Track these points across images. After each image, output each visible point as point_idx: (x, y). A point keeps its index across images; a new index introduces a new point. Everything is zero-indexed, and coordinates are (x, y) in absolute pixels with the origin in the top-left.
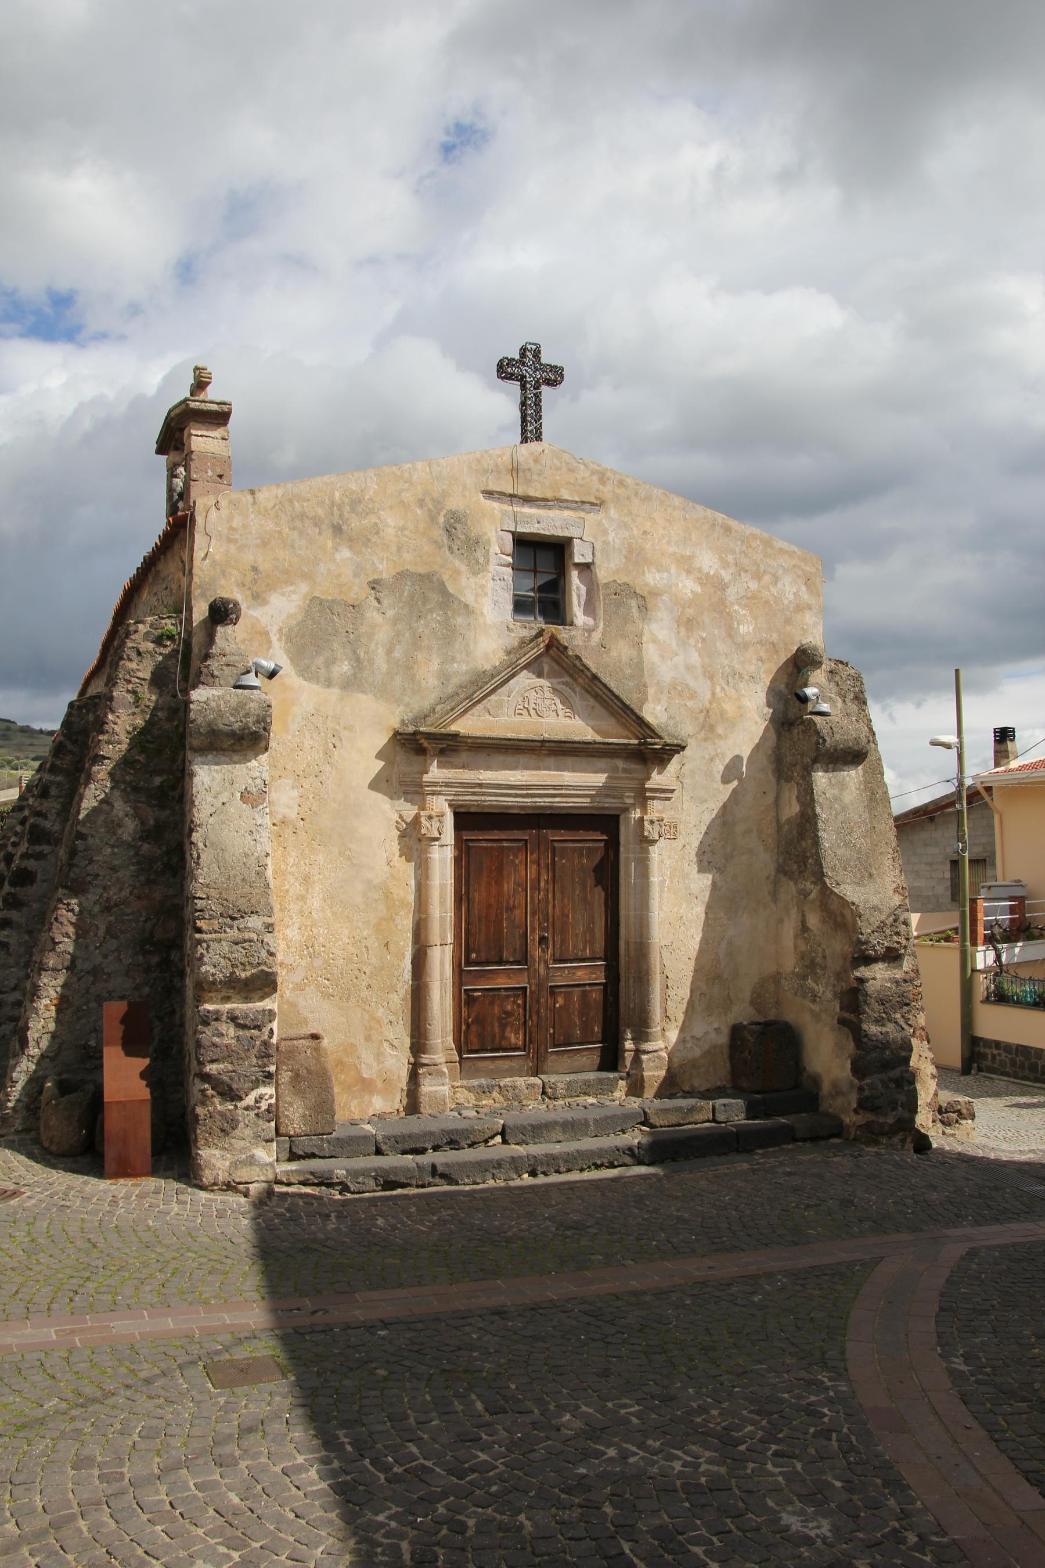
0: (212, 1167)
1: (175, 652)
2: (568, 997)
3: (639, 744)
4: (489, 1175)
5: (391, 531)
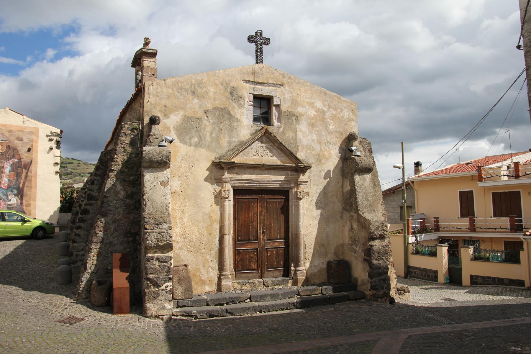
0: (151, 310)
1: (138, 134)
2: (272, 252)
4: (245, 313)
5: (212, 93)
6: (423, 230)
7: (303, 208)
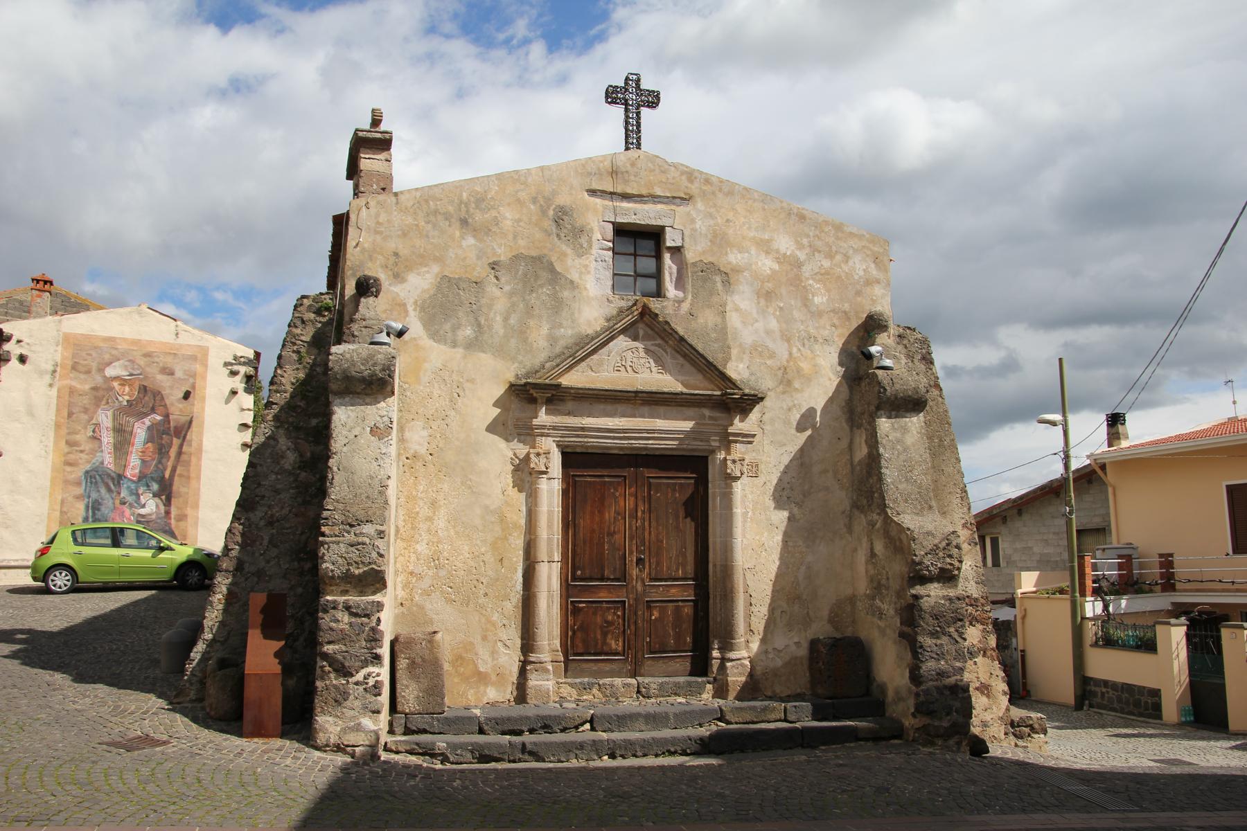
0: (325, 731)
1: (330, 321)
2: (663, 611)
3: (722, 395)
4: (572, 755)
5: (509, 223)
6: (1128, 584)
7: (743, 501)
